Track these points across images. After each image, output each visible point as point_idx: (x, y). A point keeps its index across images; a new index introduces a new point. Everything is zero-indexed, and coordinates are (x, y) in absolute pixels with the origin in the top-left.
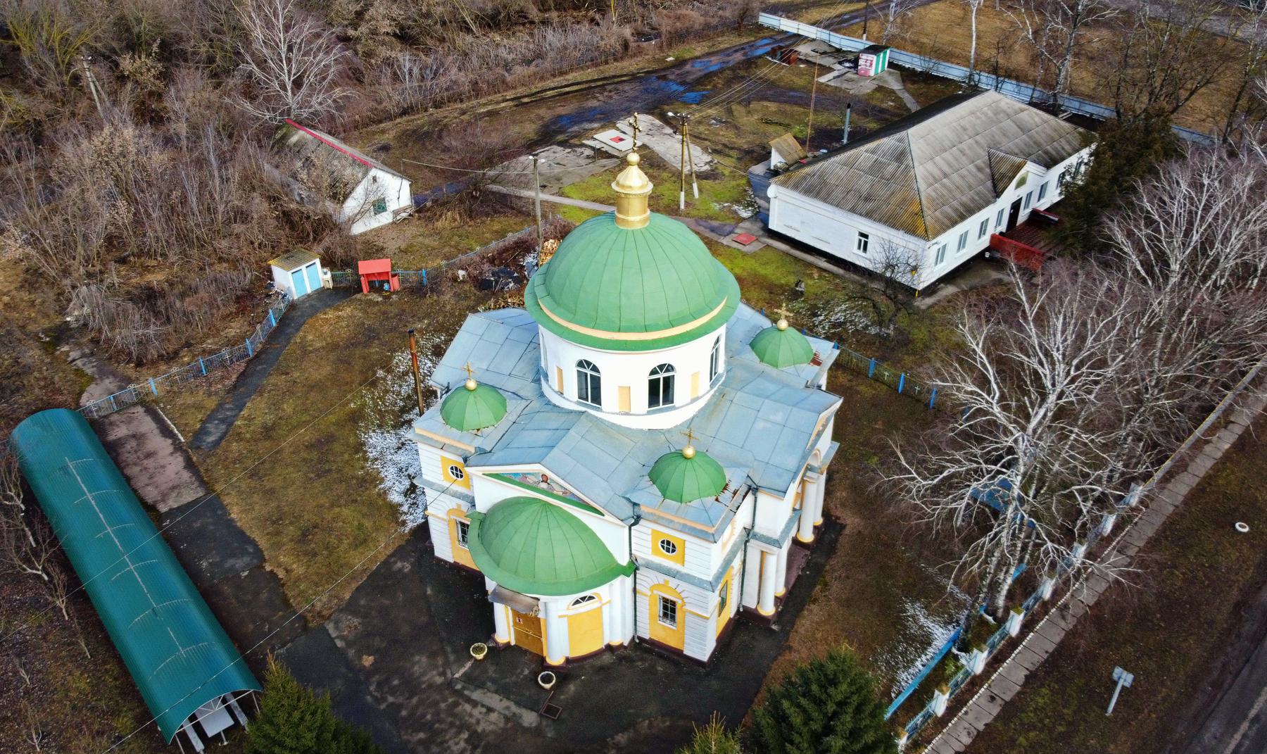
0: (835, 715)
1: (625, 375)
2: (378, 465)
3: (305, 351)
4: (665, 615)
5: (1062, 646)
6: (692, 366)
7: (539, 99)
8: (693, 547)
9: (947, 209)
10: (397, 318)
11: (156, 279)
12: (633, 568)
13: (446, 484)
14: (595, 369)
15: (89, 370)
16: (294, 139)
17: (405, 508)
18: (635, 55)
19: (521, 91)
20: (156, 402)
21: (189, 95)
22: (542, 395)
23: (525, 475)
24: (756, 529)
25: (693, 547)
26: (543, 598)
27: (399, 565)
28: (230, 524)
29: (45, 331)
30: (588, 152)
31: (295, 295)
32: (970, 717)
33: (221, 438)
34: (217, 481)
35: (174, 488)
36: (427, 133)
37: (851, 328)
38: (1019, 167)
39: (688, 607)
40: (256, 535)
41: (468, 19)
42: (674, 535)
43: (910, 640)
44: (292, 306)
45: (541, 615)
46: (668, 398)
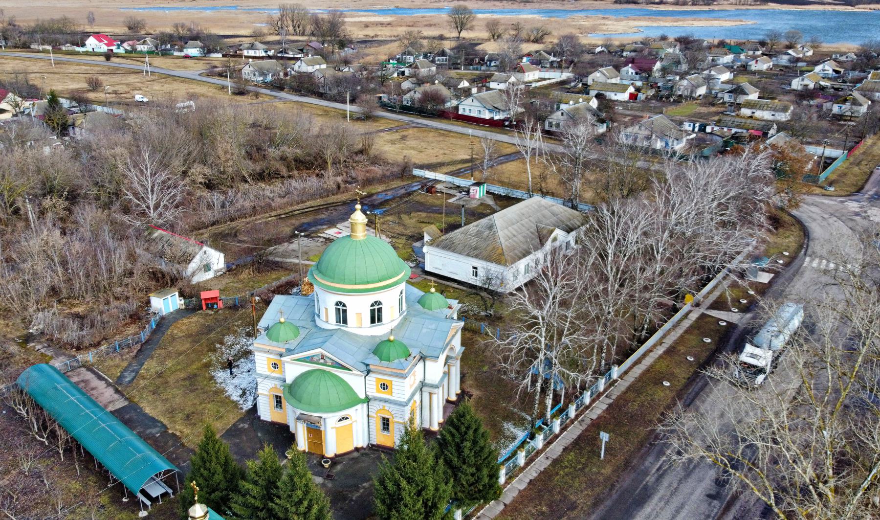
0: (466, 433)
1: (358, 307)
2: (223, 385)
3: (174, 338)
4: (384, 428)
5: (579, 437)
6: (391, 301)
7: (290, 215)
8: (396, 383)
9: (516, 251)
10: (226, 321)
11: (80, 310)
12: (368, 400)
13: (268, 373)
14: (344, 305)
15: (49, 353)
16: (155, 235)
17: (241, 402)
18: (344, 192)
19: (279, 212)
20: (92, 365)
21: (88, 215)
22: (316, 326)
23: (312, 357)
24: (426, 381)
25: (396, 383)
26: (324, 415)
27: (242, 425)
28: (145, 415)
29: (19, 337)
30: (321, 240)
31: (164, 313)
32: (537, 466)
33: (133, 379)
34: (134, 397)
35: (110, 402)
36: (228, 234)
37: (471, 313)
38: (552, 231)
39: (396, 420)
40: (161, 419)
41: (246, 175)
42: (386, 379)
43: (507, 438)
44: (163, 318)
45: (322, 429)
46: (380, 320)
